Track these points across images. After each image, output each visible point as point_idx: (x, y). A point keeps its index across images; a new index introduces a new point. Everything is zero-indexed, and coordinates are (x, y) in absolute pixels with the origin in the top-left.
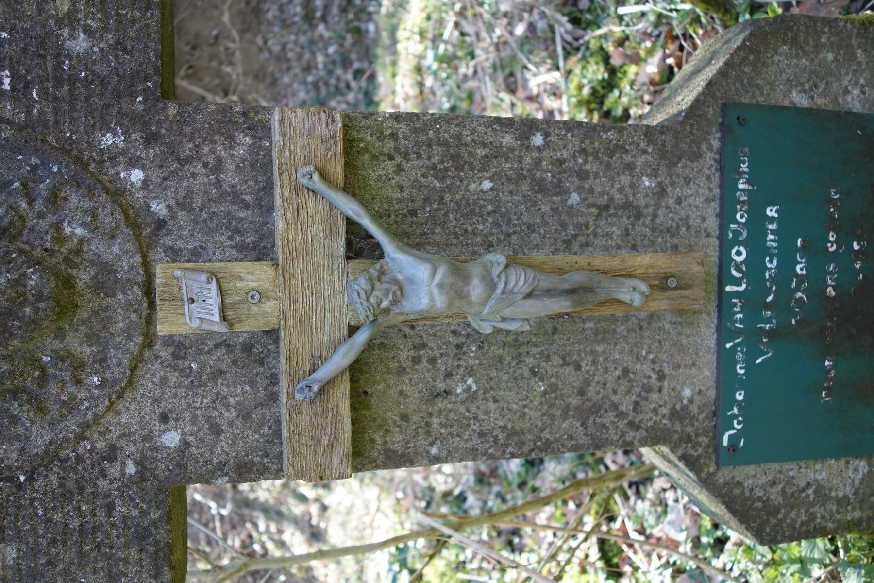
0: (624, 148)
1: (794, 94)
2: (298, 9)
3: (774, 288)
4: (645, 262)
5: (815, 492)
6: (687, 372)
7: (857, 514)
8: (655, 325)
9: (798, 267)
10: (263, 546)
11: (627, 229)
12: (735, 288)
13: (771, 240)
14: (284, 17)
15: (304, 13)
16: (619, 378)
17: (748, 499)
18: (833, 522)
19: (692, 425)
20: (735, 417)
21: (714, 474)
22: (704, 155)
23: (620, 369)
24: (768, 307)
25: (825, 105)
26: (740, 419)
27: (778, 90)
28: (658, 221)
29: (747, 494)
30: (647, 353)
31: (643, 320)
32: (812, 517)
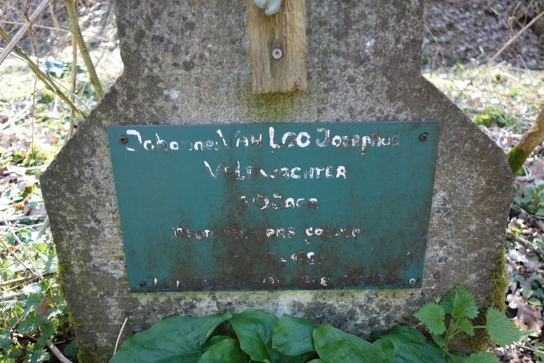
0: (402, 18)
1: (443, 194)
2: (439, 26)
3: (272, 177)
4: (296, 21)
5: (92, 228)
6: (194, 94)
7: (77, 270)
8: (236, 57)
9: (291, 200)
10: (85, 14)
11: (325, 23)
12: (272, 137)
13: (315, 172)
14: (434, 17)
15: (437, 29)
16: (185, 19)
17: (81, 161)
18: (67, 247)
19: (144, 101)
20: (154, 142)
21: (100, 125)
22: (392, 104)
23: (193, 20)
24: (256, 171)
25: (432, 224)
26: (153, 147)
27: (447, 178)
28: (333, 58)
29: (85, 161)
30: (210, 49)
31: (241, 44)
32: (71, 228)
